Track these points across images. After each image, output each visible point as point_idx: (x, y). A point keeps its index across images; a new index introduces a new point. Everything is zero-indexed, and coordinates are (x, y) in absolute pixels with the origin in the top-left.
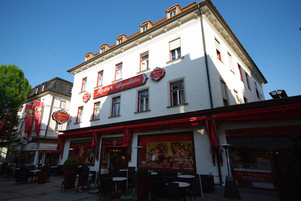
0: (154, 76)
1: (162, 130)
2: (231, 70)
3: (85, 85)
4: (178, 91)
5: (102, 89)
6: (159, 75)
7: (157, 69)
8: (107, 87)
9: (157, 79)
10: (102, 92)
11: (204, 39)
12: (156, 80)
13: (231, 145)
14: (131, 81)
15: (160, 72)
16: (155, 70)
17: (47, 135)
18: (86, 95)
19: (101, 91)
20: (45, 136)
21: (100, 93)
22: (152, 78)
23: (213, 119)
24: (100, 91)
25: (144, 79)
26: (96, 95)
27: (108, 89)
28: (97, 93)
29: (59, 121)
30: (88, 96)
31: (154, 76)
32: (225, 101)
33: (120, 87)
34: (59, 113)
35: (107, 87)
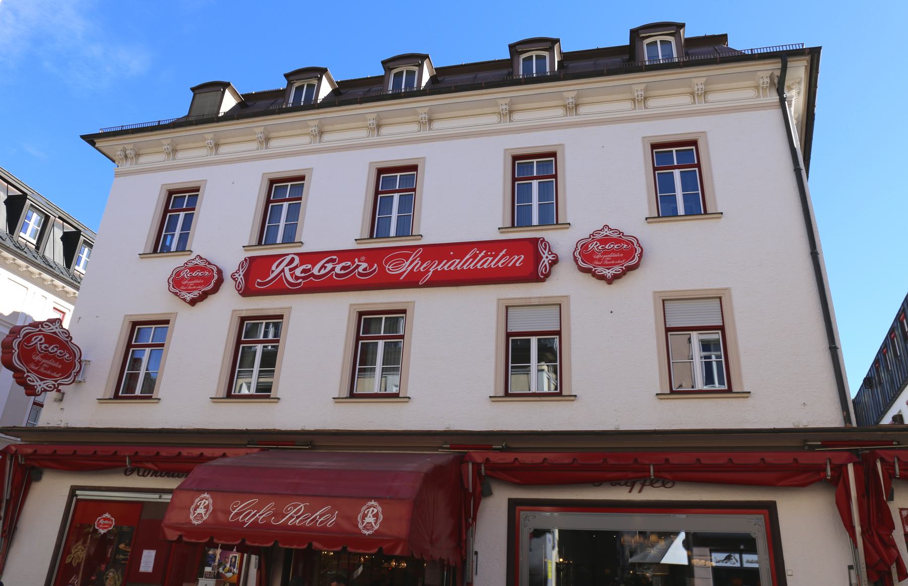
5: (302, 263)
6: (200, 284)
9: (189, 297)
13: (82, 540)
30: (207, 281)
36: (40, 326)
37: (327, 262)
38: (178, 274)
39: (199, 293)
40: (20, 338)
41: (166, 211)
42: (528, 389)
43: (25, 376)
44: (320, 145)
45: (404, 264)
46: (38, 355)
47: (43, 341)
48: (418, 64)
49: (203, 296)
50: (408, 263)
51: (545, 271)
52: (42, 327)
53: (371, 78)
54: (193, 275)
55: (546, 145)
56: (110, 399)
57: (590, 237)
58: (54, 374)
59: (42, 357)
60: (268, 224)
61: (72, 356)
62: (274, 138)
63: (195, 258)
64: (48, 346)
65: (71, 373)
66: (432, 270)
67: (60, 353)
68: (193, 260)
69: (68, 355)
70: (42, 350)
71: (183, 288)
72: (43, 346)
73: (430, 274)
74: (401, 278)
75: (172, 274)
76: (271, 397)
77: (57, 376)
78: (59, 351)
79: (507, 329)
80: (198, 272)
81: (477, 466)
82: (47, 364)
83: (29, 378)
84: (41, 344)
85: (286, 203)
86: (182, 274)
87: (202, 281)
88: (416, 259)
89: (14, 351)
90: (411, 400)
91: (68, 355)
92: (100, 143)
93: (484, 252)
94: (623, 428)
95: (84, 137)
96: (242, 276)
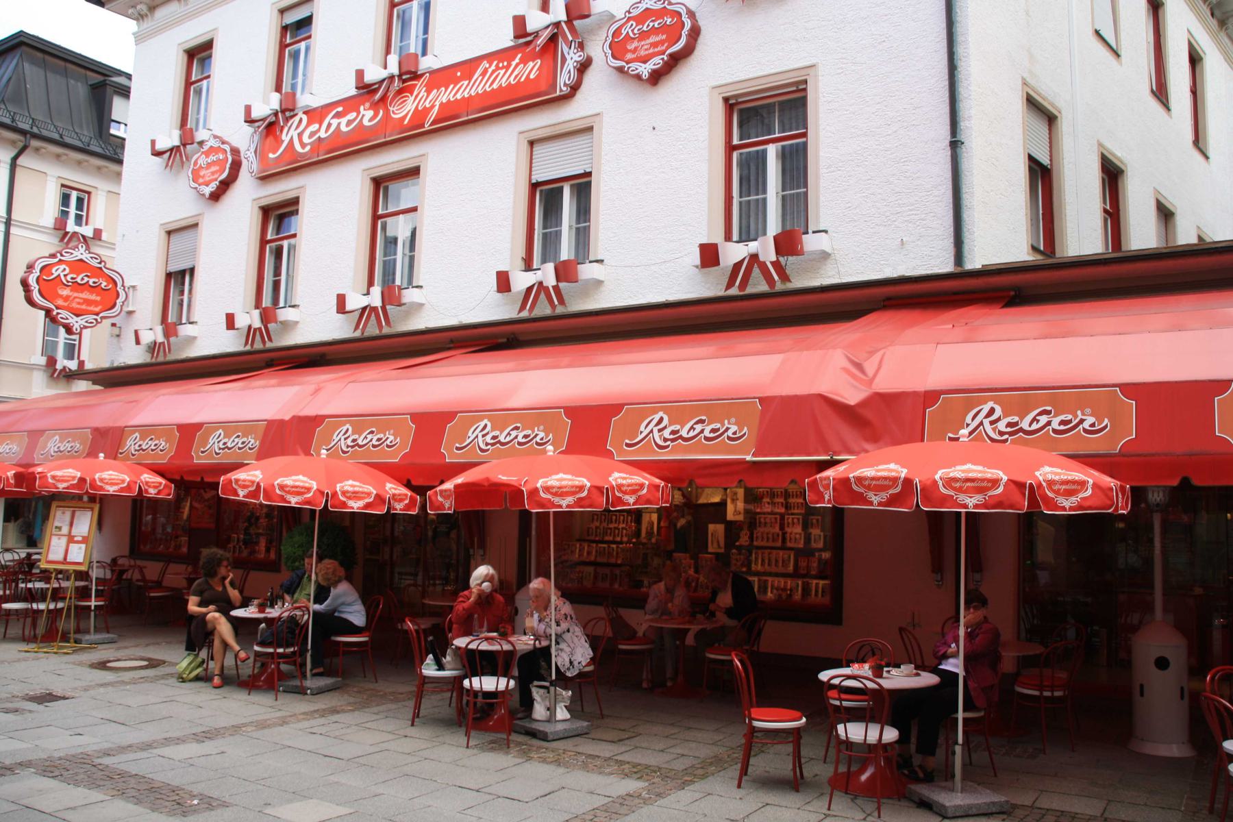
2: (1097, 33)
3: (199, 92)
4: (772, 151)
6: (662, 42)
8: (340, 109)
9: (645, 69)
12: (638, 77)
15: (663, 29)
16: (635, 13)
18: (212, 158)
19: (300, 135)
21: (298, 147)
22: (619, 63)
24: (294, 133)
25: (570, 65)
26: (271, 156)
27: (344, 121)
28: (280, 146)
29: (64, 313)
31: (631, 47)
32: (450, 683)
33: (420, 115)
34: (63, 266)
35: (340, 109)
36: (58, 255)
47: (67, 271)
49: (675, 61)
51: (569, 79)
54: (645, 29)
66: (437, 103)
72: (1001, 426)
73: (437, 108)
74: (406, 122)
79: (530, 175)
83: (60, 316)
84: (65, 276)
86: (199, 162)
87: (664, 37)
93: (495, 63)
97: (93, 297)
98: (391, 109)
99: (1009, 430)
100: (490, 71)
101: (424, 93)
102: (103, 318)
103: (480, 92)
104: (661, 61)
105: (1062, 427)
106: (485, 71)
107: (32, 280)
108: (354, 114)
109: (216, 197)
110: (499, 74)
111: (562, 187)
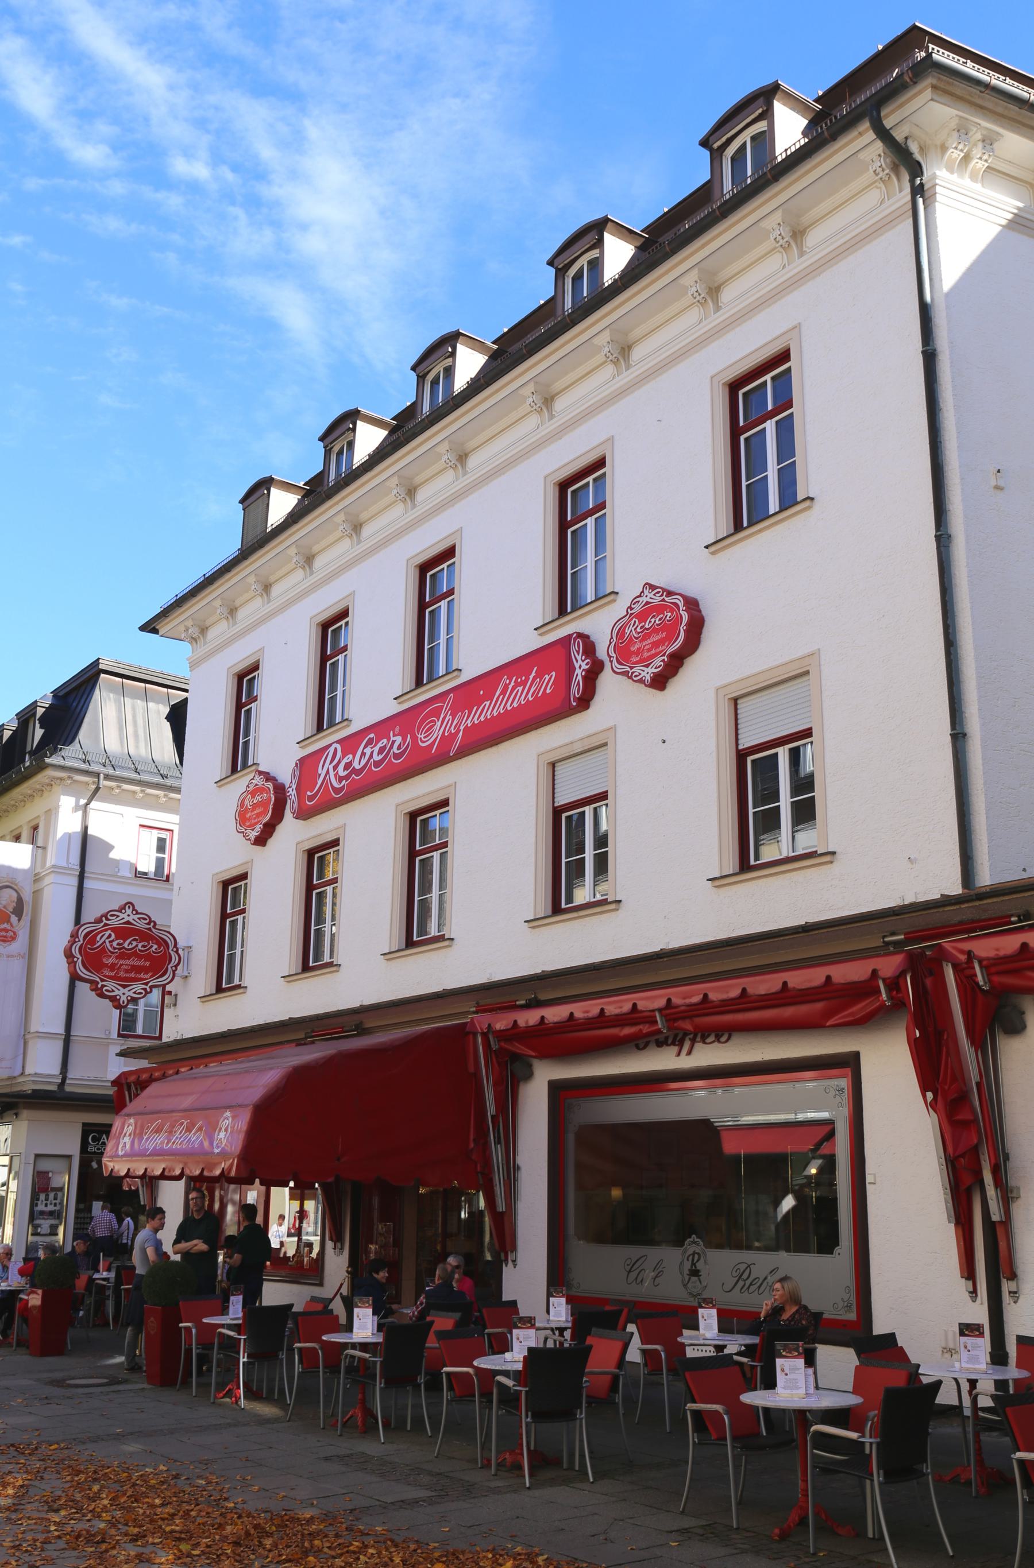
0: (634, 648)
1: (687, 1045)
5: (344, 756)
7: (649, 596)
10: (639, 630)
11: (930, 359)
14: (503, 692)
17: (75, 1073)
19: (335, 768)
20: (64, 1080)
23: (688, 1413)
33: (447, 740)
36: (104, 919)
37: (365, 747)
38: (621, 633)
39: (663, 661)
40: (79, 941)
41: (735, 432)
42: (778, 854)
43: (99, 986)
44: (361, 547)
45: (435, 727)
46: (111, 956)
48: (448, 354)
49: (676, 663)
50: (439, 724)
52: (107, 919)
53: (510, 330)
55: (774, 336)
56: (211, 995)
57: (628, 613)
58: (142, 976)
59: (117, 958)
60: (747, 481)
61: (162, 945)
62: (561, 392)
63: (643, 592)
64: (122, 941)
65: (167, 969)
67: (143, 946)
68: (640, 596)
69: (155, 946)
70: (115, 948)
71: (634, 659)
72: (115, 944)
75: (612, 638)
76: (334, 963)
77: (146, 976)
78: (140, 945)
79: (737, 744)
80: (654, 616)
81: (964, 973)
82: (126, 965)
83: (105, 988)
84: (110, 942)
85: (769, 422)
86: (627, 631)
88: (448, 712)
89: (75, 959)
90: (455, 942)
91: (155, 946)
92: (164, 627)
94: (675, 944)
95: (143, 628)
96: (577, 666)
97: (141, 963)
98: (419, 736)
99: (118, 947)
100: (510, 687)
101: (449, 717)
102: (151, 987)
103: (523, 703)
104: (662, 663)
105: (143, 949)
106: (506, 686)
107: (76, 951)
108: (385, 741)
109: (261, 841)
110: (518, 691)
111: (776, 754)
